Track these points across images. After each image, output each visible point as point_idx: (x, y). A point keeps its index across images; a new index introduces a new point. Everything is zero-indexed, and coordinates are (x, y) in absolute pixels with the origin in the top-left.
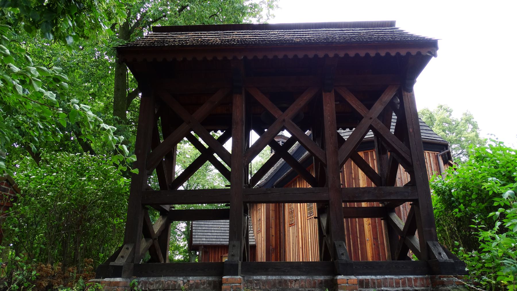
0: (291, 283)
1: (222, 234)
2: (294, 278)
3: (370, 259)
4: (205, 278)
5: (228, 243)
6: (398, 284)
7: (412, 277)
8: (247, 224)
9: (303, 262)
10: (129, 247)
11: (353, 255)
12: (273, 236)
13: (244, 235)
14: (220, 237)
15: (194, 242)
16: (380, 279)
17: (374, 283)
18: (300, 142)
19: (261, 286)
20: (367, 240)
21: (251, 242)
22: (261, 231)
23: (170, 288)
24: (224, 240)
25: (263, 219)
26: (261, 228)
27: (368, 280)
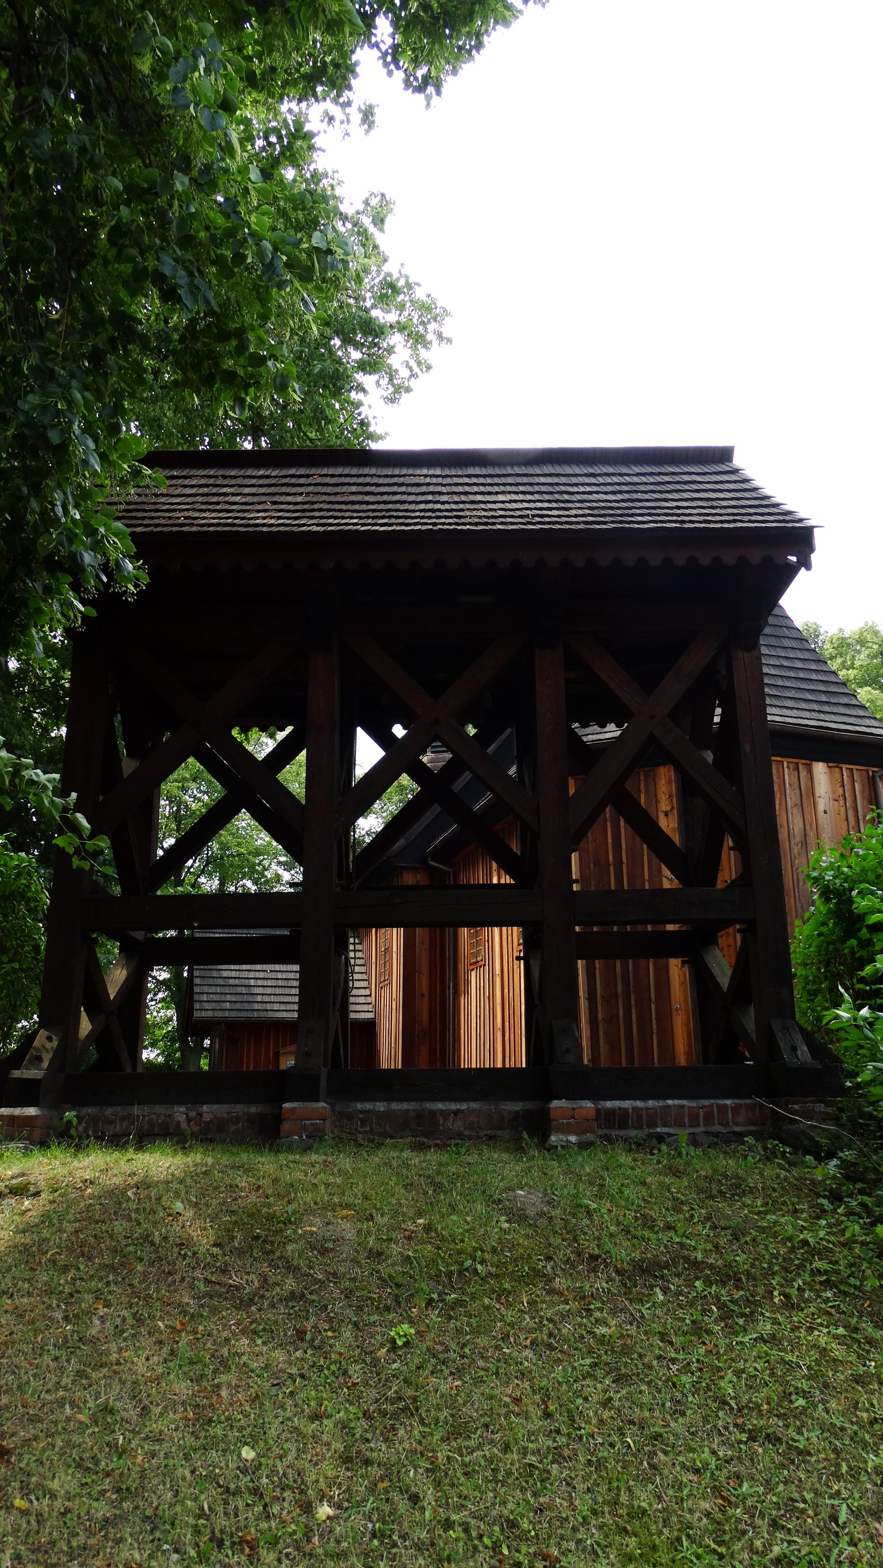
0: (445, 1119)
1: (278, 991)
2: (453, 1106)
3: (682, 1060)
4: (239, 1109)
5: (296, 1015)
6: (694, 1120)
7: (728, 1102)
8: (343, 974)
9: (504, 1068)
10: (54, 1037)
11: (636, 1049)
12: (423, 996)
13: (334, 1004)
14: (273, 998)
15: (197, 1014)
16: (654, 1109)
17: (640, 1118)
18: (472, 771)
19: (374, 1126)
20: (677, 1009)
21: (360, 1010)
22: (391, 983)
23: (156, 1130)
24: (283, 1007)
25: (395, 949)
26: (391, 975)
27: (626, 1110)
